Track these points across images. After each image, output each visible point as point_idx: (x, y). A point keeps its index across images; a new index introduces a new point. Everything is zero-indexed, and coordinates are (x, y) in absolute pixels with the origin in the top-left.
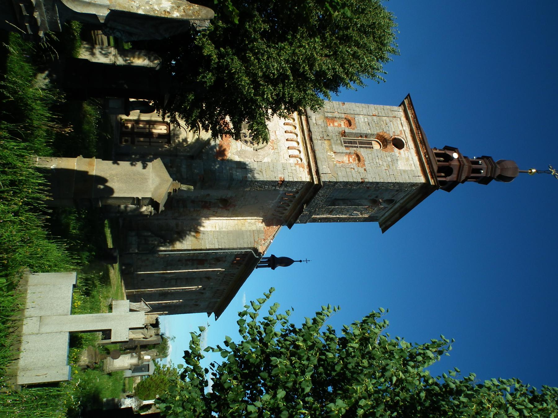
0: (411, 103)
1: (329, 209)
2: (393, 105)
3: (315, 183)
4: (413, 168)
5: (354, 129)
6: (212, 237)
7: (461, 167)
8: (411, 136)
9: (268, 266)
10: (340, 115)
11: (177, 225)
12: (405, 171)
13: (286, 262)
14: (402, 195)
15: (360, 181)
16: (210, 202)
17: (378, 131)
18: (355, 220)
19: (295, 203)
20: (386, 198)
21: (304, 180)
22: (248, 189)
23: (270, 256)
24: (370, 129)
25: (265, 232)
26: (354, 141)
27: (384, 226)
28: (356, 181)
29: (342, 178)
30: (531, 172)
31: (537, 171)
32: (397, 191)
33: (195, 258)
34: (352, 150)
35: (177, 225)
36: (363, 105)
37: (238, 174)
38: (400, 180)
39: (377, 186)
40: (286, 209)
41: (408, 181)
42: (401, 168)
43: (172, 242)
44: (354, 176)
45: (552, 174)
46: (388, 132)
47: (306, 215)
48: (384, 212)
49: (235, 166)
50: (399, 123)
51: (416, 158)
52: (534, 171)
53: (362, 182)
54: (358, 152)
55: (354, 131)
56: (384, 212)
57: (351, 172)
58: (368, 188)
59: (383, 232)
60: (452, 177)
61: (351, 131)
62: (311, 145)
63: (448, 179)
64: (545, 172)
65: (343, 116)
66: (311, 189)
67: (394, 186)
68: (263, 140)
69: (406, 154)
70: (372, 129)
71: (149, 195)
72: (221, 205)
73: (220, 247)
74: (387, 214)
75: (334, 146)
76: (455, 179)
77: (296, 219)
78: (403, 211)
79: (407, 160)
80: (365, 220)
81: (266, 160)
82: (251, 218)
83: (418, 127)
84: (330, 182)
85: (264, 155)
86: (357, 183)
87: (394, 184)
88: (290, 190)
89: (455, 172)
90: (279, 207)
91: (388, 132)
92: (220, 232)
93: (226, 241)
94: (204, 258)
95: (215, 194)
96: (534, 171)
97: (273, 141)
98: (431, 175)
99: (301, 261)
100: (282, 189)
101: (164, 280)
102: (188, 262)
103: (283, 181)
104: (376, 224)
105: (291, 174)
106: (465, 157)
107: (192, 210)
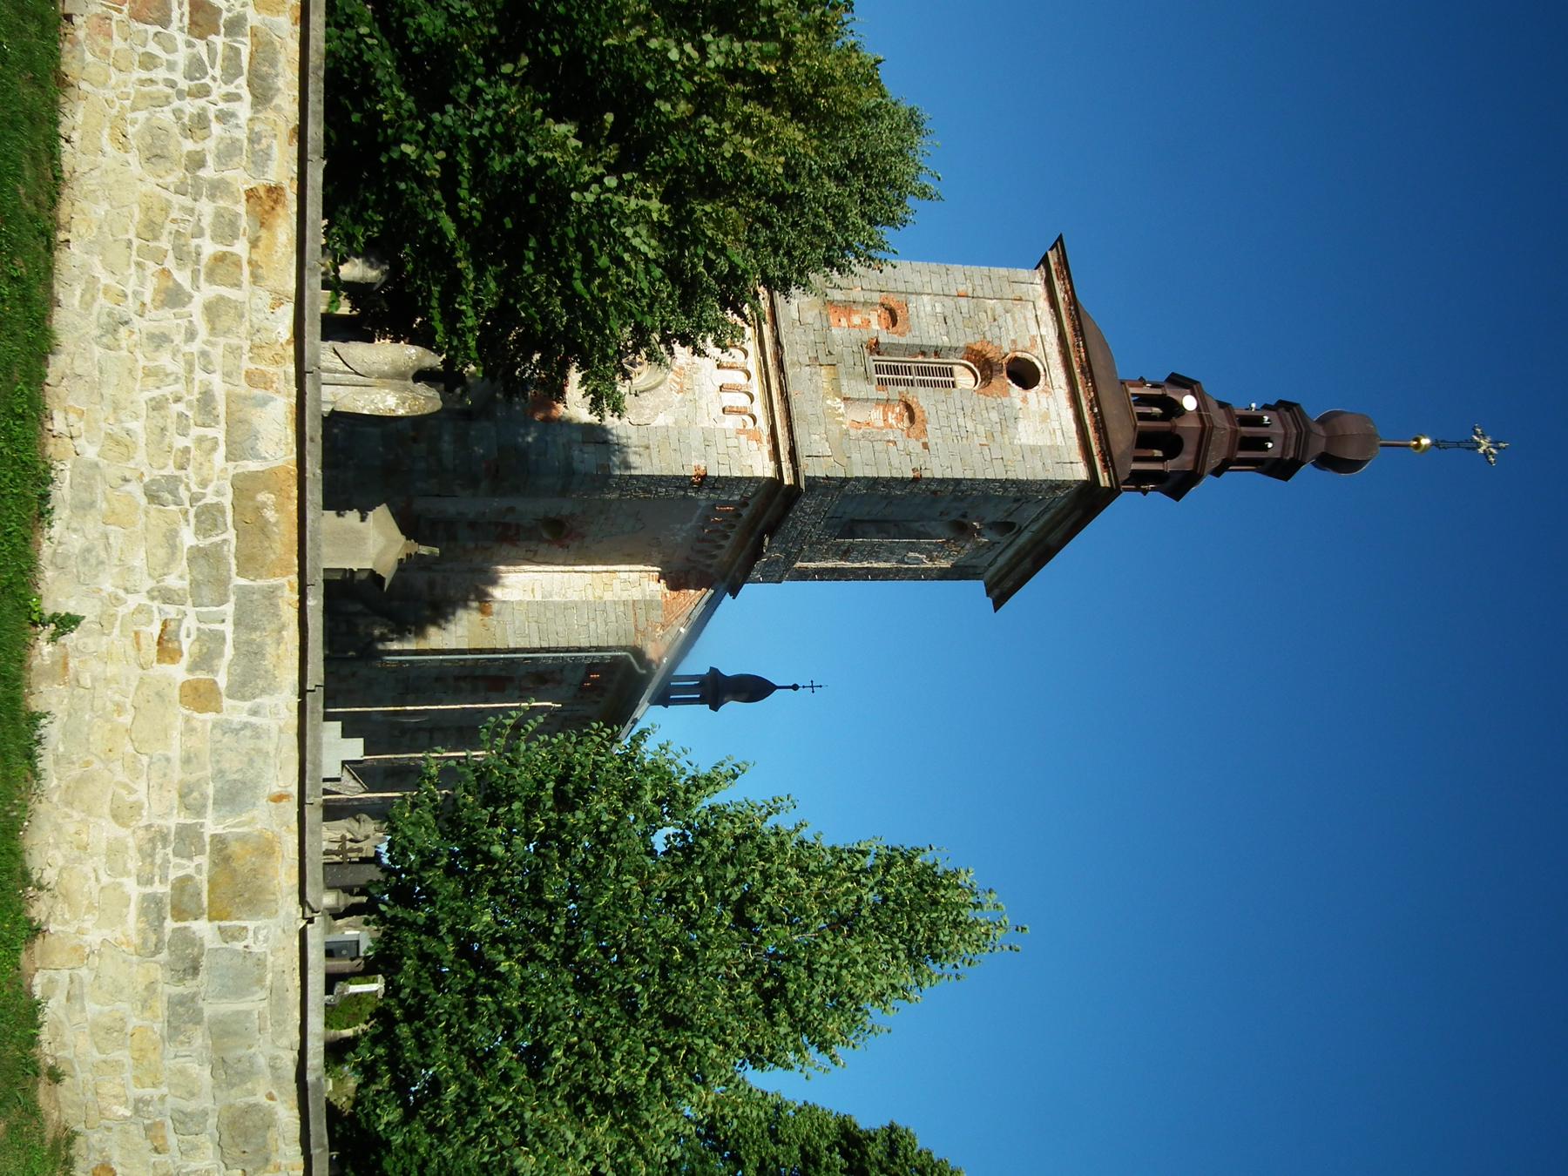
0: (1064, 262)
1: (839, 545)
3: (787, 482)
4: (1059, 440)
5: (902, 334)
6: (523, 618)
7: (1205, 434)
9: (701, 701)
10: (868, 295)
11: (431, 584)
12: (1033, 449)
13: (754, 689)
14: (1032, 511)
15: (911, 475)
16: (518, 526)
17: (970, 340)
18: (915, 575)
19: (741, 532)
20: (989, 519)
21: (758, 473)
22: (615, 496)
23: (705, 671)
24: (948, 334)
25: (666, 607)
26: (903, 368)
27: (996, 592)
28: (896, 474)
29: (861, 467)
30: (1418, 446)
31: (1435, 444)
32: (1016, 500)
33: (478, 672)
34: (894, 392)
35: (431, 584)
36: (933, 266)
37: (585, 459)
38: (1020, 472)
39: (956, 489)
40: (721, 547)
41: (1041, 476)
42: (1024, 441)
43: (420, 632)
44: (895, 462)
45: (1481, 451)
46: (996, 342)
47: (777, 560)
48: (993, 554)
49: (577, 436)
50: (1030, 315)
51: (1068, 414)
52: (1425, 441)
53: (915, 480)
54: (910, 398)
55: (903, 341)
56: (993, 554)
57: (887, 451)
58: (935, 492)
59: (996, 610)
60: (1184, 461)
61: (896, 339)
63: (1170, 466)
64: (1458, 444)
65: (876, 297)
66: (778, 499)
67: (1006, 490)
68: (614, 411)
69: (1043, 401)
70: (954, 336)
71: (369, 566)
72: (546, 535)
73: (545, 645)
74: (1001, 560)
75: (844, 382)
76: (1189, 468)
77: (750, 568)
78: (1041, 554)
79: (1045, 417)
80: (944, 575)
81: (661, 420)
82: (627, 568)
83: (1079, 331)
84: (827, 478)
85: (657, 407)
86: (903, 482)
87: (1004, 483)
88: (724, 497)
89: (1190, 447)
90: (703, 540)
91: (996, 342)
92: (544, 605)
93: (560, 629)
94: (503, 673)
95: (530, 508)
96: (1425, 441)
97: (682, 368)
98: (1103, 460)
99: (795, 687)
100: (702, 496)
101: (396, 733)
102: (463, 684)
103: (704, 477)
104: (978, 586)
105: (725, 460)
106: (1222, 405)
107: (471, 545)
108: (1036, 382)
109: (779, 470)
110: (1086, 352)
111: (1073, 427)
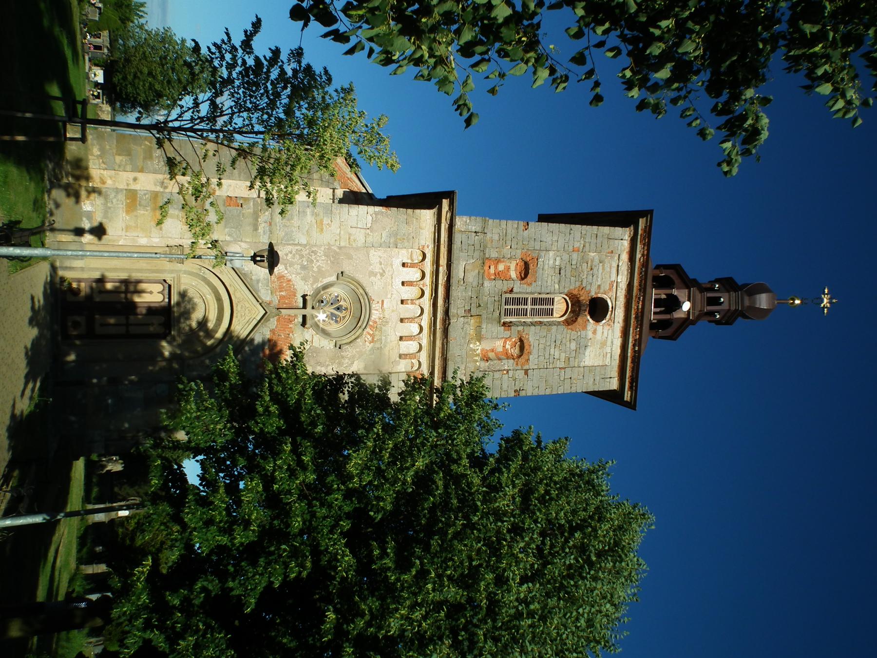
2: (615, 226)
8: (626, 296)
30: (793, 303)
50: (615, 265)
51: (618, 342)
52: (797, 302)
62: (443, 344)
85: (353, 357)
96: (797, 302)
98: (631, 383)
108: (603, 317)
109: (432, 374)
110: (643, 305)
111: (618, 351)
